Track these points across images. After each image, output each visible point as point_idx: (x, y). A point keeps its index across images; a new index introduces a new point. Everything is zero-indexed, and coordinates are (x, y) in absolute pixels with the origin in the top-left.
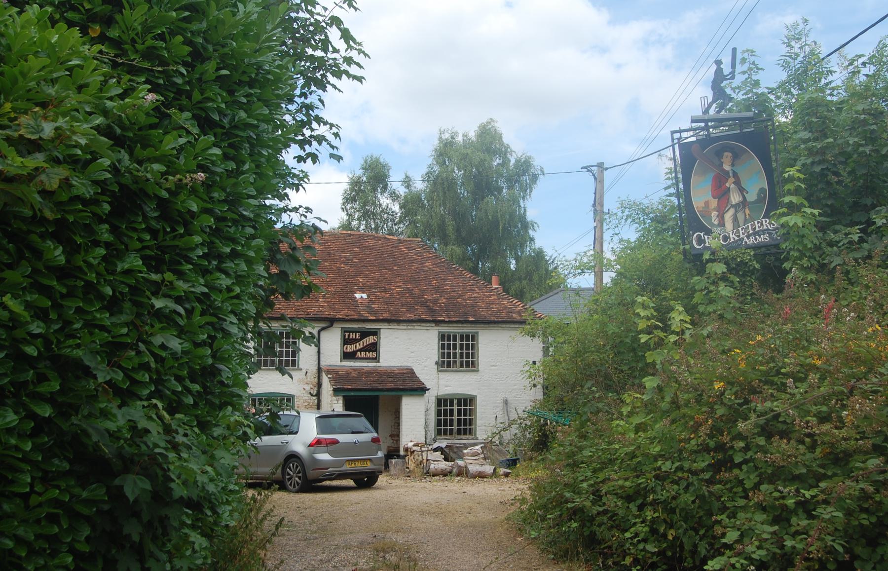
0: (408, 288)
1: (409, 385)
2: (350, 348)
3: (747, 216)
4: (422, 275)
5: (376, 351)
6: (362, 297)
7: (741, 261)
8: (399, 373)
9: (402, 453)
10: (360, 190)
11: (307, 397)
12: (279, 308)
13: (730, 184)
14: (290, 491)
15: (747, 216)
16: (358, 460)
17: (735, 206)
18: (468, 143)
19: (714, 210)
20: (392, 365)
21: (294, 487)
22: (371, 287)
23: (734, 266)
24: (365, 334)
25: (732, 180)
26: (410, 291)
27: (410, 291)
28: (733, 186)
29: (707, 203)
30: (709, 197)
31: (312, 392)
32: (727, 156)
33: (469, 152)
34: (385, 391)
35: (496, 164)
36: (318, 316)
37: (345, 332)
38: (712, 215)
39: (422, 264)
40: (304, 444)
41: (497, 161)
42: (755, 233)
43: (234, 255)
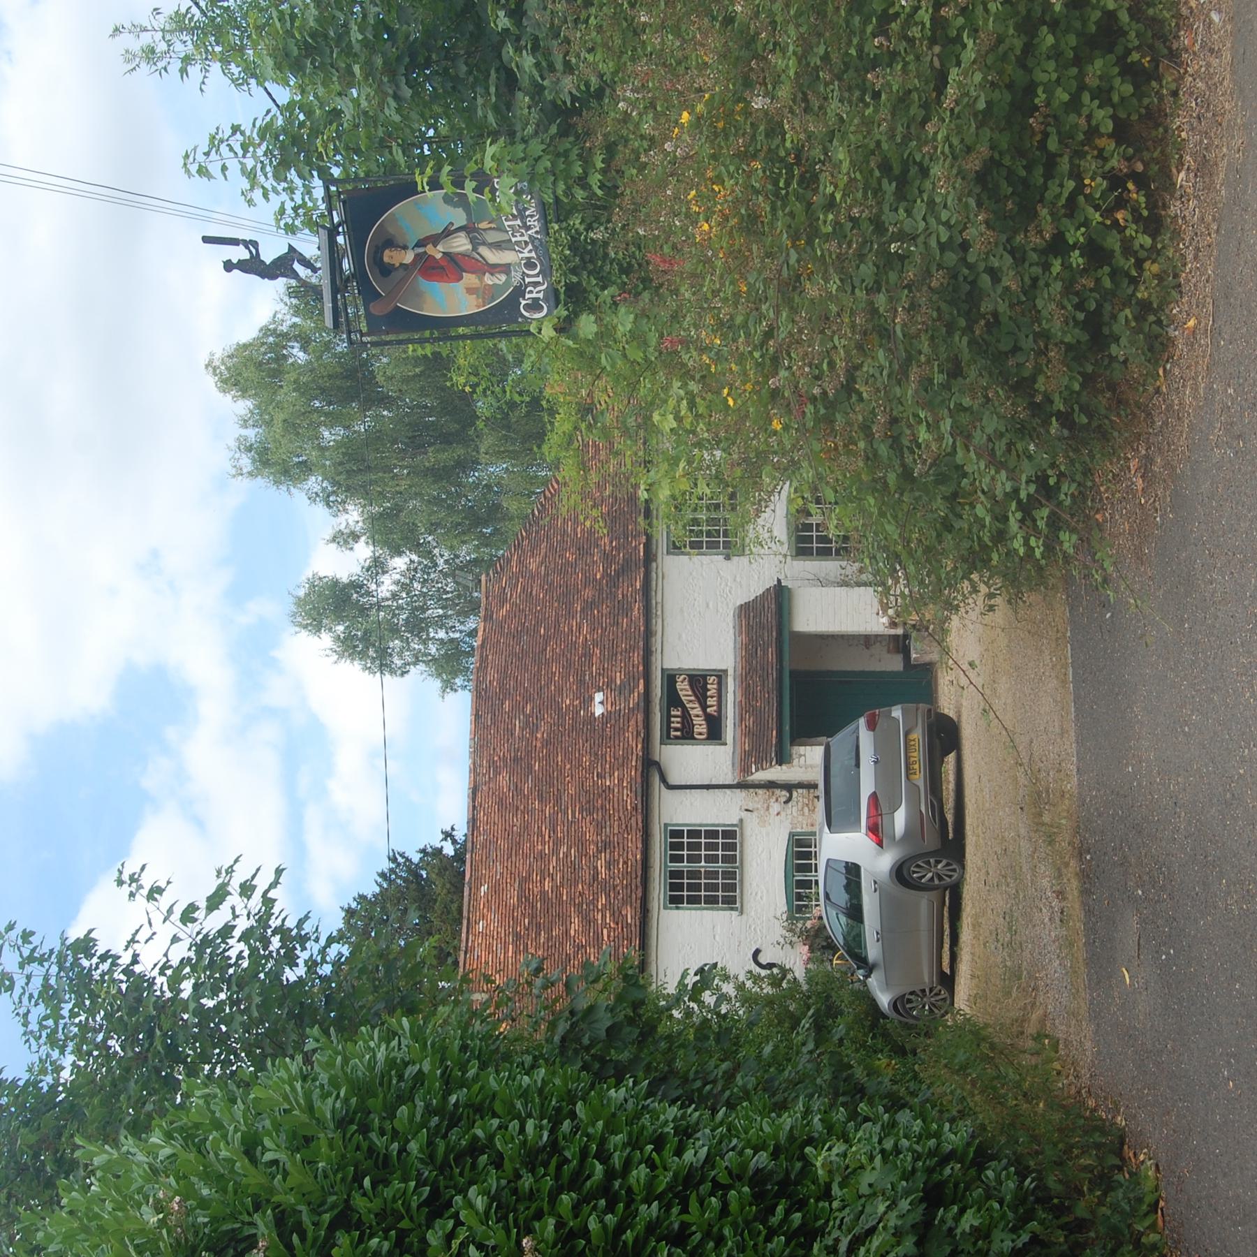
0: (583, 610)
1: (770, 618)
2: (700, 727)
3: (493, 225)
4: (556, 579)
5: (704, 677)
6: (602, 703)
7: (570, 249)
8: (748, 634)
9: (900, 631)
10: (363, 639)
11: (793, 809)
12: (625, 863)
13: (437, 252)
14: (962, 877)
15: (493, 225)
16: (907, 769)
17: (475, 244)
18: (262, 417)
19: (481, 280)
20: (732, 645)
21: (954, 870)
22: (581, 682)
23: (577, 259)
24: (673, 699)
25: (430, 249)
26: (589, 606)
27: (589, 606)
28: (440, 248)
29: (470, 291)
30: (459, 287)
31: (784, 799)
32: (389, 256)
33: (280, 417)
34: (781, 665)
35: (301, 354)
36: (639, 790)
37: (668, 737)
38: (490, 283)
39: (533, 577)
40: (879, 854)
41: (298, 355)
42: (521, 215)
43: (604, 1157)
